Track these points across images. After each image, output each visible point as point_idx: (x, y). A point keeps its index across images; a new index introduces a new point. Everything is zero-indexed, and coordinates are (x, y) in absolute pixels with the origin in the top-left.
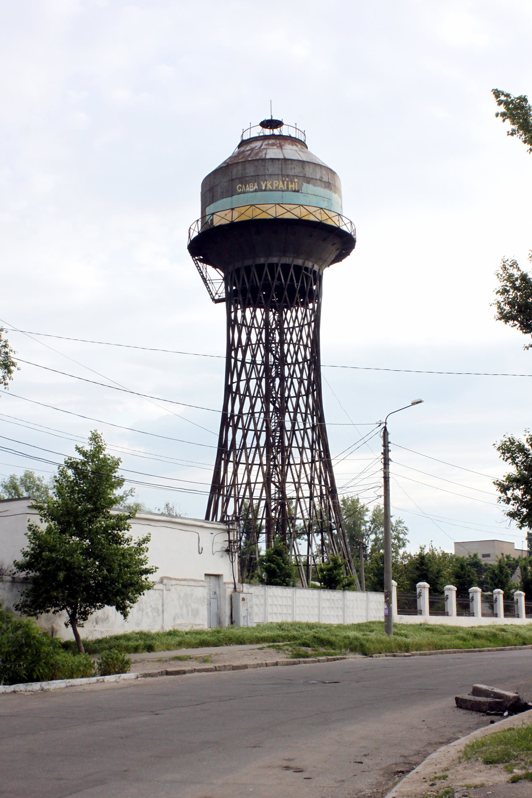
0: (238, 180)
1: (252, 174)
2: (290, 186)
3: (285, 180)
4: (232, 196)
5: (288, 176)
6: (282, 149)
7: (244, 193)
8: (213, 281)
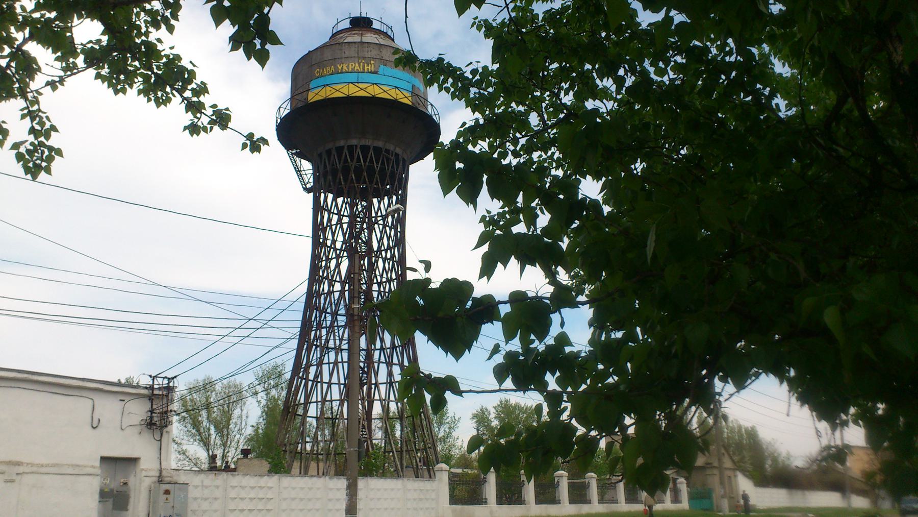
5: (364, 58)
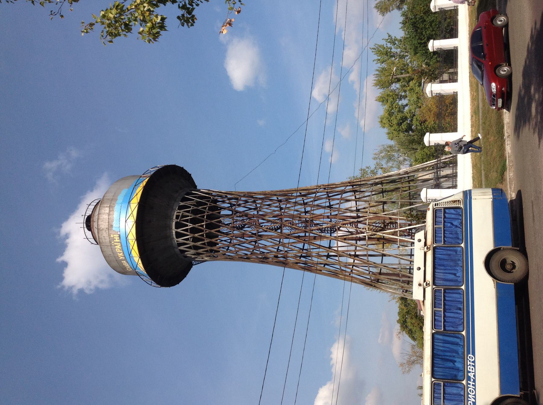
2: (117, 241)
5: (110, 242)
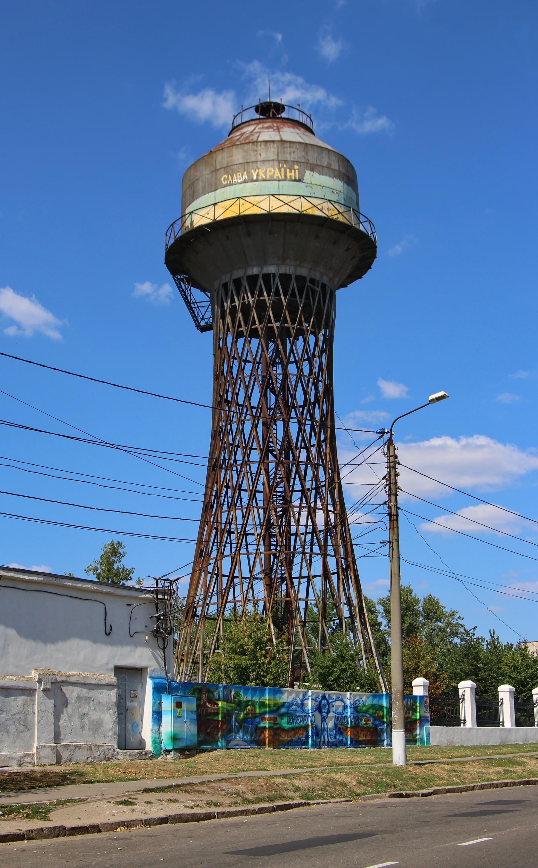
0: (223, 170)
1: (241, 161)
2: (289, 174)
3: (283, 167)
4: (215, 190)
6: (279, 131)
7: (231, 185)
8: (199, 305)
